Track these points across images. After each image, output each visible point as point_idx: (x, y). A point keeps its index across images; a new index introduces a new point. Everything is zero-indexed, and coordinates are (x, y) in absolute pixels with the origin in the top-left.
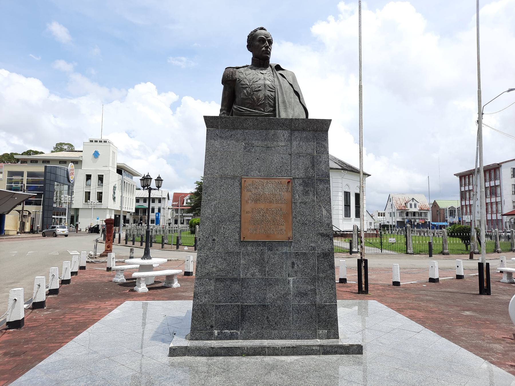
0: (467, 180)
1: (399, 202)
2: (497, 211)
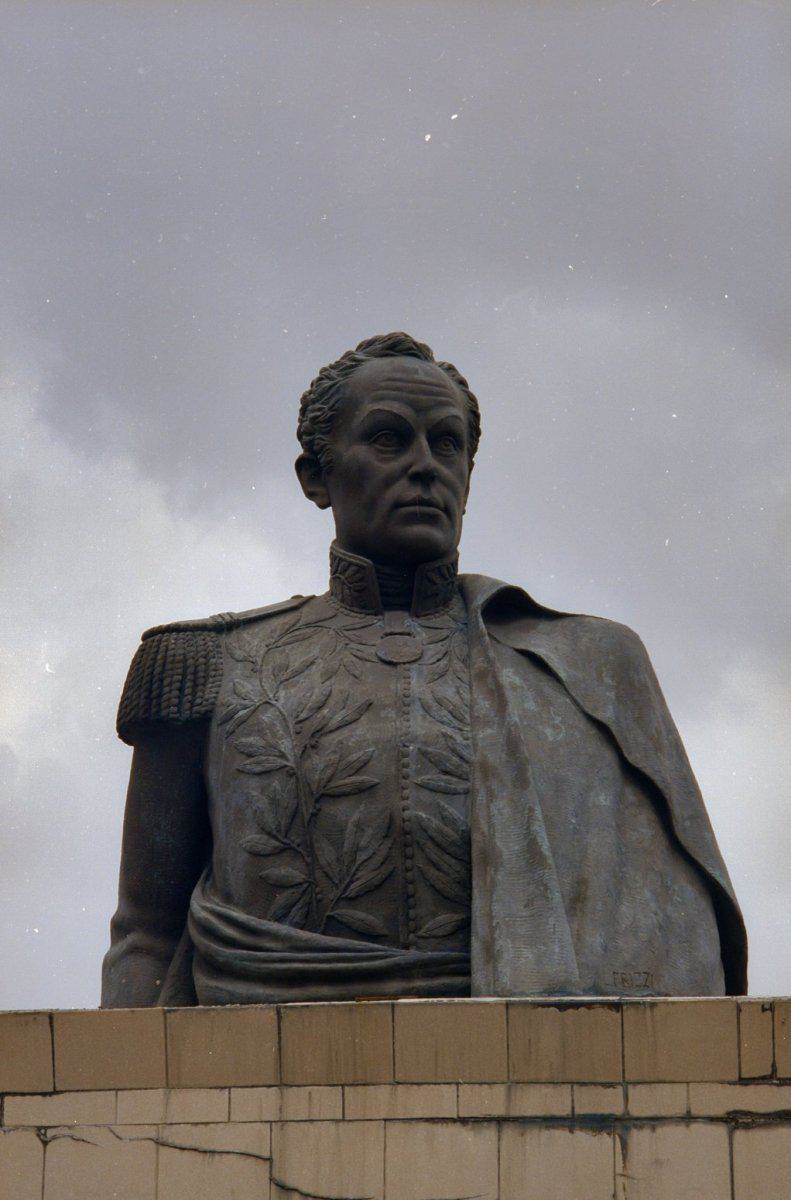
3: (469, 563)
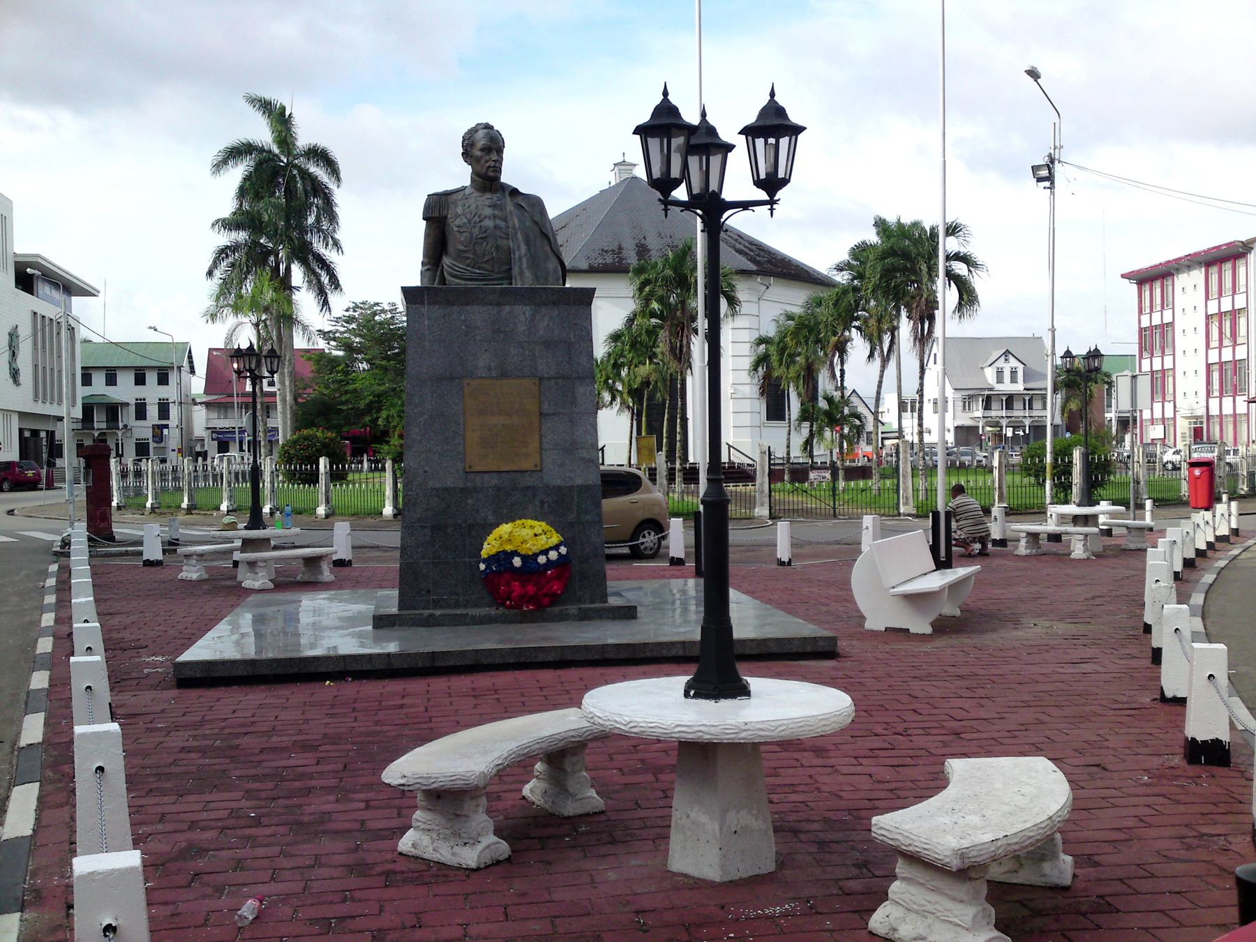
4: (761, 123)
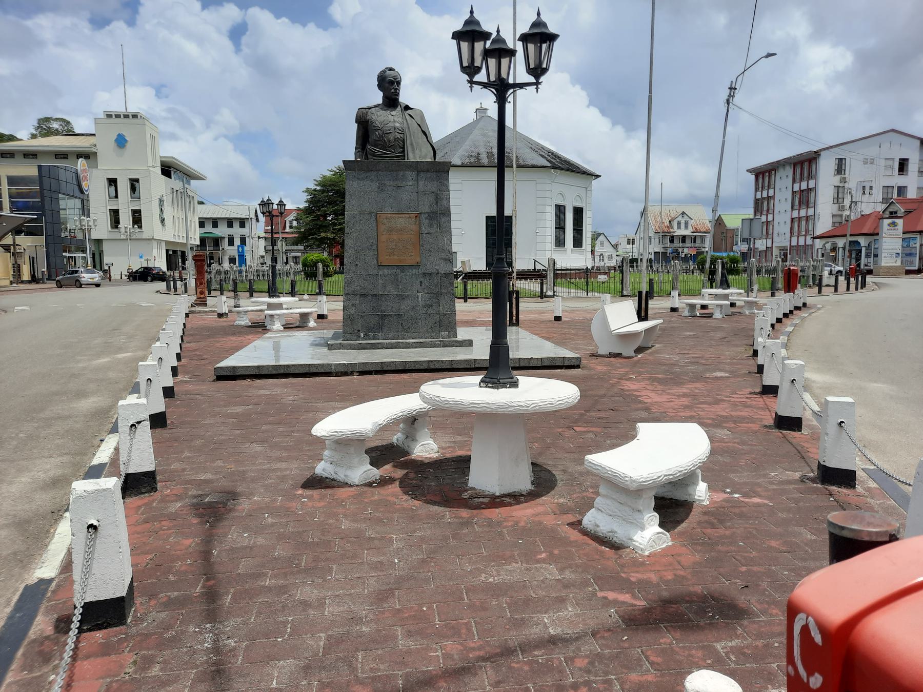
0: (767, 179)
1: (659, 219)
2: (807, 231)
3: (400, 100)
4: (531, 32)
